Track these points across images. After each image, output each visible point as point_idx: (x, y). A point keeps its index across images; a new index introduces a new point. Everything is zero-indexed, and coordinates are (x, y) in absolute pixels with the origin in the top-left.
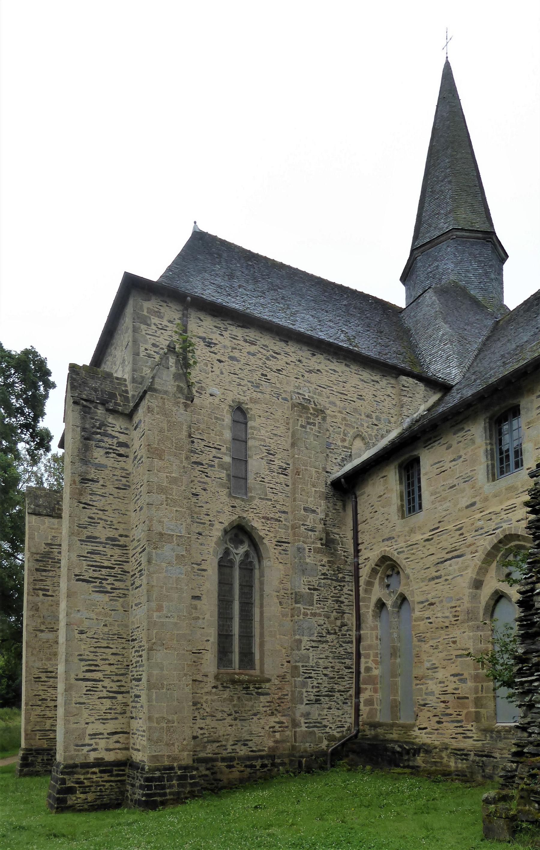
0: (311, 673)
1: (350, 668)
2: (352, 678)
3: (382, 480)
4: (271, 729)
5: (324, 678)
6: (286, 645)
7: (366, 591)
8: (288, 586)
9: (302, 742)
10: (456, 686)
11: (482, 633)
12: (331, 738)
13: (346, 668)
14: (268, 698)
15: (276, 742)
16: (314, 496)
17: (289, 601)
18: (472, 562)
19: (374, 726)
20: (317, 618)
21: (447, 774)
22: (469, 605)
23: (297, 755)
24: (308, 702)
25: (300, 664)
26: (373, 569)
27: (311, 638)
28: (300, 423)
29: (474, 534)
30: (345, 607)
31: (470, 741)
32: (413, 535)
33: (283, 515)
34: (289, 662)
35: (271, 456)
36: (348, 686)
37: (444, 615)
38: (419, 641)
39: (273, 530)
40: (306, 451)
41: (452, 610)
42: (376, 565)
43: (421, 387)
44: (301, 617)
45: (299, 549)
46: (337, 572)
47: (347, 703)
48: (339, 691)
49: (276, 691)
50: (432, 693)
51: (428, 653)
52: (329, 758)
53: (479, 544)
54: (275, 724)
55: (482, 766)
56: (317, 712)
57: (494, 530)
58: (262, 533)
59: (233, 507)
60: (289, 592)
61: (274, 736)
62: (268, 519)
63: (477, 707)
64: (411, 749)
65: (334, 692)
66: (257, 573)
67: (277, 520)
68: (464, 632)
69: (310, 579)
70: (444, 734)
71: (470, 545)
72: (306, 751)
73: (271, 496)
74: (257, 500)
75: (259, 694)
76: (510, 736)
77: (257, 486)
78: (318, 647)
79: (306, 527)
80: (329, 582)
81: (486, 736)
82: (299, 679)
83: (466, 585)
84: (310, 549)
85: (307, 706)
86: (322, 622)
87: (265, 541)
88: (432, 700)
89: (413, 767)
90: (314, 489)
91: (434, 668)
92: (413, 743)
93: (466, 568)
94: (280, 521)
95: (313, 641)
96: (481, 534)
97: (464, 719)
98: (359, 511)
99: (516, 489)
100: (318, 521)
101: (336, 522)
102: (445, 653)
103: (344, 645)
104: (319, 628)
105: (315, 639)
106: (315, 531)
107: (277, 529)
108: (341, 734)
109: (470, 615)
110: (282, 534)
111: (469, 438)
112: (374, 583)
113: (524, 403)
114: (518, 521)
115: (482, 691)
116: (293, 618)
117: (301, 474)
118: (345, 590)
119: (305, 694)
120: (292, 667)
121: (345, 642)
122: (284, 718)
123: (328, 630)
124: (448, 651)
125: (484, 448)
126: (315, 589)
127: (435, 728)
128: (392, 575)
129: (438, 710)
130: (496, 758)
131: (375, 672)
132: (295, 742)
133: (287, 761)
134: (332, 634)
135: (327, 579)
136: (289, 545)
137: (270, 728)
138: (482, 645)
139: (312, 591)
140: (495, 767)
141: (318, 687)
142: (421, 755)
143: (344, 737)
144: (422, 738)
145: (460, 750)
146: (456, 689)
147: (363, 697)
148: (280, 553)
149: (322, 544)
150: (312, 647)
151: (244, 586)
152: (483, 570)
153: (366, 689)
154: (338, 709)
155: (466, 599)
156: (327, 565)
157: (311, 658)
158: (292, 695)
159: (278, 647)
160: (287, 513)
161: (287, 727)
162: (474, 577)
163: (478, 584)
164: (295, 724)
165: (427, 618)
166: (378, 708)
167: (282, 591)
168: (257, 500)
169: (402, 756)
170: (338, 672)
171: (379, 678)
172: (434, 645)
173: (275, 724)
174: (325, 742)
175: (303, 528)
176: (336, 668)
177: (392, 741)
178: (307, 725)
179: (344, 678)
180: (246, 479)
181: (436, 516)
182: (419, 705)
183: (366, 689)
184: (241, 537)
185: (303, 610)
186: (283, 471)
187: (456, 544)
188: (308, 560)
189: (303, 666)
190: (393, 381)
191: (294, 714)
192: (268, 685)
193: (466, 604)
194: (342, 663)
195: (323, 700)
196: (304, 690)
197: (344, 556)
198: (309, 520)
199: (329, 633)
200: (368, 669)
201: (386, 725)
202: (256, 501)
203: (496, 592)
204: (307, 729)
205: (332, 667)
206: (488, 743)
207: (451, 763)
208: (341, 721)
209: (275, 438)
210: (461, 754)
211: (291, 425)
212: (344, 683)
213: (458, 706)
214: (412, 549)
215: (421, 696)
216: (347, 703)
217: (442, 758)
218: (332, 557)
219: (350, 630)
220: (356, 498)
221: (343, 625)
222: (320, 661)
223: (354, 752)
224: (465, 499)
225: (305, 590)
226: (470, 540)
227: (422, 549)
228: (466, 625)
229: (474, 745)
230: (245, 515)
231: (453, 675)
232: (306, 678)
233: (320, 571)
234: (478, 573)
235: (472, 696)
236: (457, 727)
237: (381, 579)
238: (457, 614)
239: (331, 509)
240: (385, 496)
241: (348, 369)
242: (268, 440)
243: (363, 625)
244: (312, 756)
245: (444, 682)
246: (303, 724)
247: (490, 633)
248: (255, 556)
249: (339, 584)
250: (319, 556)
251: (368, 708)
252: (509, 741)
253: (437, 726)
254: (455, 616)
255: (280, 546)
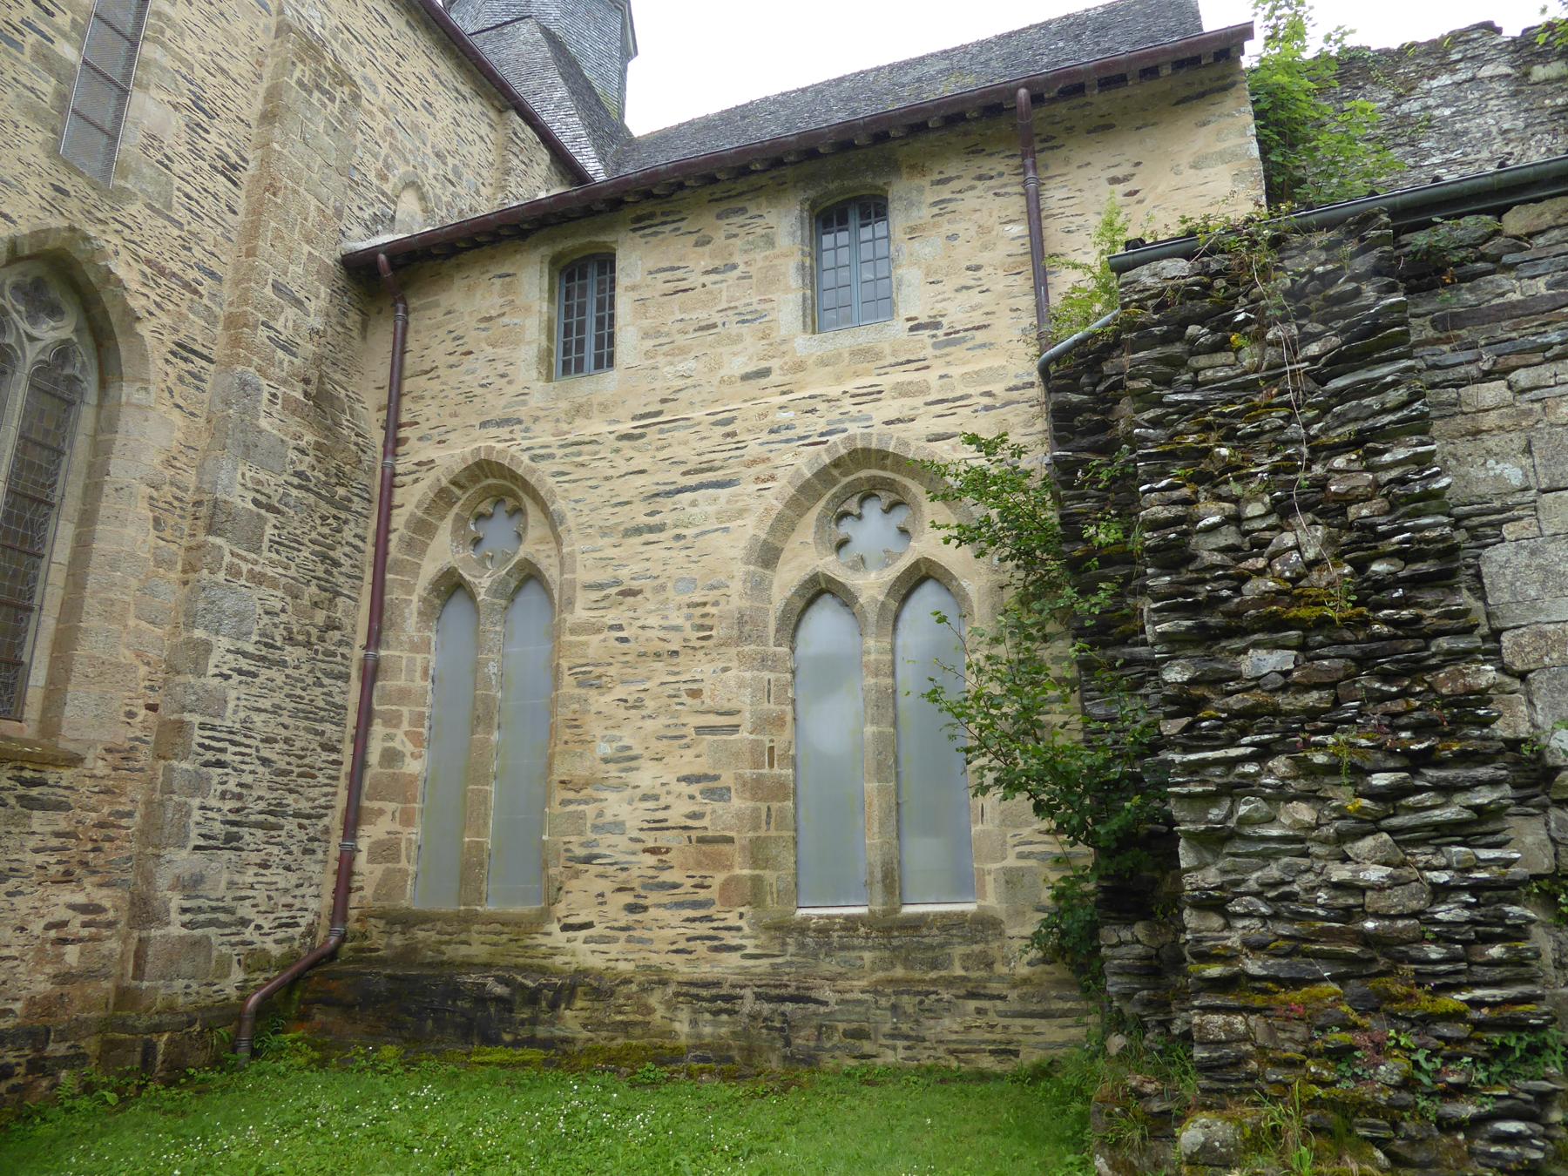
0: (223, 750)
1: (334, 750)
2: (336, 778)
3: (498, 282)
4: (53, 933)
5: (261, 769)
6: (152, 655)
7: (410, 545)
8: (190, 478)
9: (162, 977)
10: (696, 808)
11: (772, 676)
12: (255, 961)
13: (324, 747)
14: (62, 822)
15: (64, 978)
16: (302, 268)
17: (186, 525)
18: (754, 507)
19: (405, 921)
20: (264, 591)
21: (668, 1057)
22: (745, 604)
23: (144, 1022)
24: (202, 842)
25: (196, 719)
26: (442, 490)
27: (239, 644)
28: (297, 74)
29: (765, 437)
30: (342, 579)
31: (734, 959)
32: (578, 422)
33: (208, 282)
34: (152, 708)
35: (201, 115)
36: (322, 801)
37: (665, 623)
38: (580, 684)
39: (171, 307)
40: (300, 147)
41: (691, 610)
42: (454, 483)
43: (544, 156)
44: (221, 576)
45: (244, 384)
46: (334, 480)
47: (313, 852)
48: (296, 815)
49: (94, 800)
50: (618, 827)
51: (609, 718)
52: (247, 1025)
53: (778, 462)
54: (67, 914)
55: (782, 1030)
56: (225, 877)
57: (822, 435)
58: (136, 303)
59: (57, 189)
60: (189, 497)
61: (60, 957)
62: (162, 272)
63: (755, 864)
64: (545, 986)
65: (284, 815)
66: (87, 417)
67: (186, 285)
68: (725, 670)
69: (262, 476)
70: (651, 941)
71: (754, 462)
72: (171, 1009)
73: (181, 214)
74: (139, 205)
75: (29, 803)
76: (856, 942)
77: (146, 170)
78: (255, 675)
79: (272, 334)
80: (312, 499)
81: (784, 944)
82: (185, 765)
83: (739, 553)
84: (274, 395)
85: (199, 855)
86: (279, 606)
87: (140, 328)
88: (614, 846)
89: (547, 1044)
90: (306, 248)
91: (626, 759)
92: (543, 971)
93: (741, 513)
94: (196, 292)
95: (245, 654)
96: (788, 441)
97: (715, 896)
98: (411, 344)
99: (878, 356)
100: (304, 331)
101: (340, 356)
102: (663, 720)
103: (326, 681)
104: (266, 619)
105: (250, 649)
106: (294, 355)
107: (184, 310)
108: (285, 947)
109: (747, 628)
110: (195, 330)
111: (759, 231)
112: (437, 528)
113: (899, 189)
114: (887, 423)
115: (768, 823)
116: (192, 576)
117: (281, 194)
118: (348, 533)
119: (197, 815)
120: (163, 724)
121: (329, 675)
122: (105, 891)
123: (289, 630)
124: (675, 715)
125: (798, 257)
126: (270, 508)
127: (622, 923)
128: (491, 515)
129: (635, 872)
130: (826, 1004)
131: (413, 767)
132: (139, 973)
133: (91, 1045)
134: (298, 644)
135: (308, 490)
136: (212, 367)
137: (48, 927)
138: (772, 706)
139: (263, 512)
140: (822, 1030)
141: (239, 797)
142: (579, 1004)
143: (293, 956)
144: (581, 954)
145: (706, 985)
146: (694, 816)
147: (369, 834)
148: (180, 379)
149: (306, 394)
150: (240, 672)
151: (36, 443)
152: (784, 524)
153: (381, 812)
154: (288, 868)
155: (736, 587)
156: (311, 452)
157: (231, 705)
158: (147, 816)
159: (126, 656)
160: (219, 280)
161: (110, 925)
162: (763, 536)
163: (768, 556)
164: (144, 911)
165: (611, 628)
166: (412, 868)
167: (166, 488)
168: (139, 205)
169: (511, 1011)
170: (301, 757)
171: (420, 784)
172: (631, 699)
173: (67, 914)
174: (238, 975)
175: (263, 333)
176: (298, 744)
177: (469, 965)
178: (187, 917)
179: (314, 777)
180: (113, 138)
181: (657, 385)
182: (570, 859)
183: (381, 812)
184: (55, 293)
185: (228, 558)
186: (230, 170)
187: (713, 456)
188: (264, 423)
189: (203, 726)
190: (493, 114)
191: (149, 879)
192: (67, 775)
193: (736, 599)
194: (317, 733)
195: (247, 837)
196: (196, 802)
197: (356, 444)
198: (282, 319)
199: (290, 639)
200: (391, 757)
201: (446, 919)
202: (136, 208)
203: (814, 579)
204: (185, 931)
205: (286, 740)
206: (790, 964)
207: (677, 1026)
208: (289, 906)
209: (221, 78)
210: (712, 997)
211: (267, 73)
212: (314, 793)
213: (699, 864)
214: (579, 454)
215: (581, 833)
216: (313, 852)
217: (650, 1011)
218: (327, 437)
219: (348, 644)
220: (406, 311)
221: (331, 626)
222: (258, 719)
223: (328, 1002)
224: (741, 359)
225: (243, 502)
226: (753, 450)
227: (611, 456)
228: (733, 651)
229: (744, 971)
230: (92, 231)
231: (688, 779)
232: (206, 764)
233: (293, 462)
234: (773, 529)
235: (743, 836)
236: (694, 920)
237: (460, 522)
238: (707, 622)
239: (334, 320)
240: (505, 320)
241: (410, 33)
242: (200, 72)
243: (389, 635)
244: (191, 1024)
245: (656, 798)
246: (175, 916)
247: (789, 676)
248: (92, 366)
249: (335, 512)
250: (294, 424)
251: (379, 869)
252: (856, 954)
253: (625, 919)
254: (701, 627)
255: (186, 360)
